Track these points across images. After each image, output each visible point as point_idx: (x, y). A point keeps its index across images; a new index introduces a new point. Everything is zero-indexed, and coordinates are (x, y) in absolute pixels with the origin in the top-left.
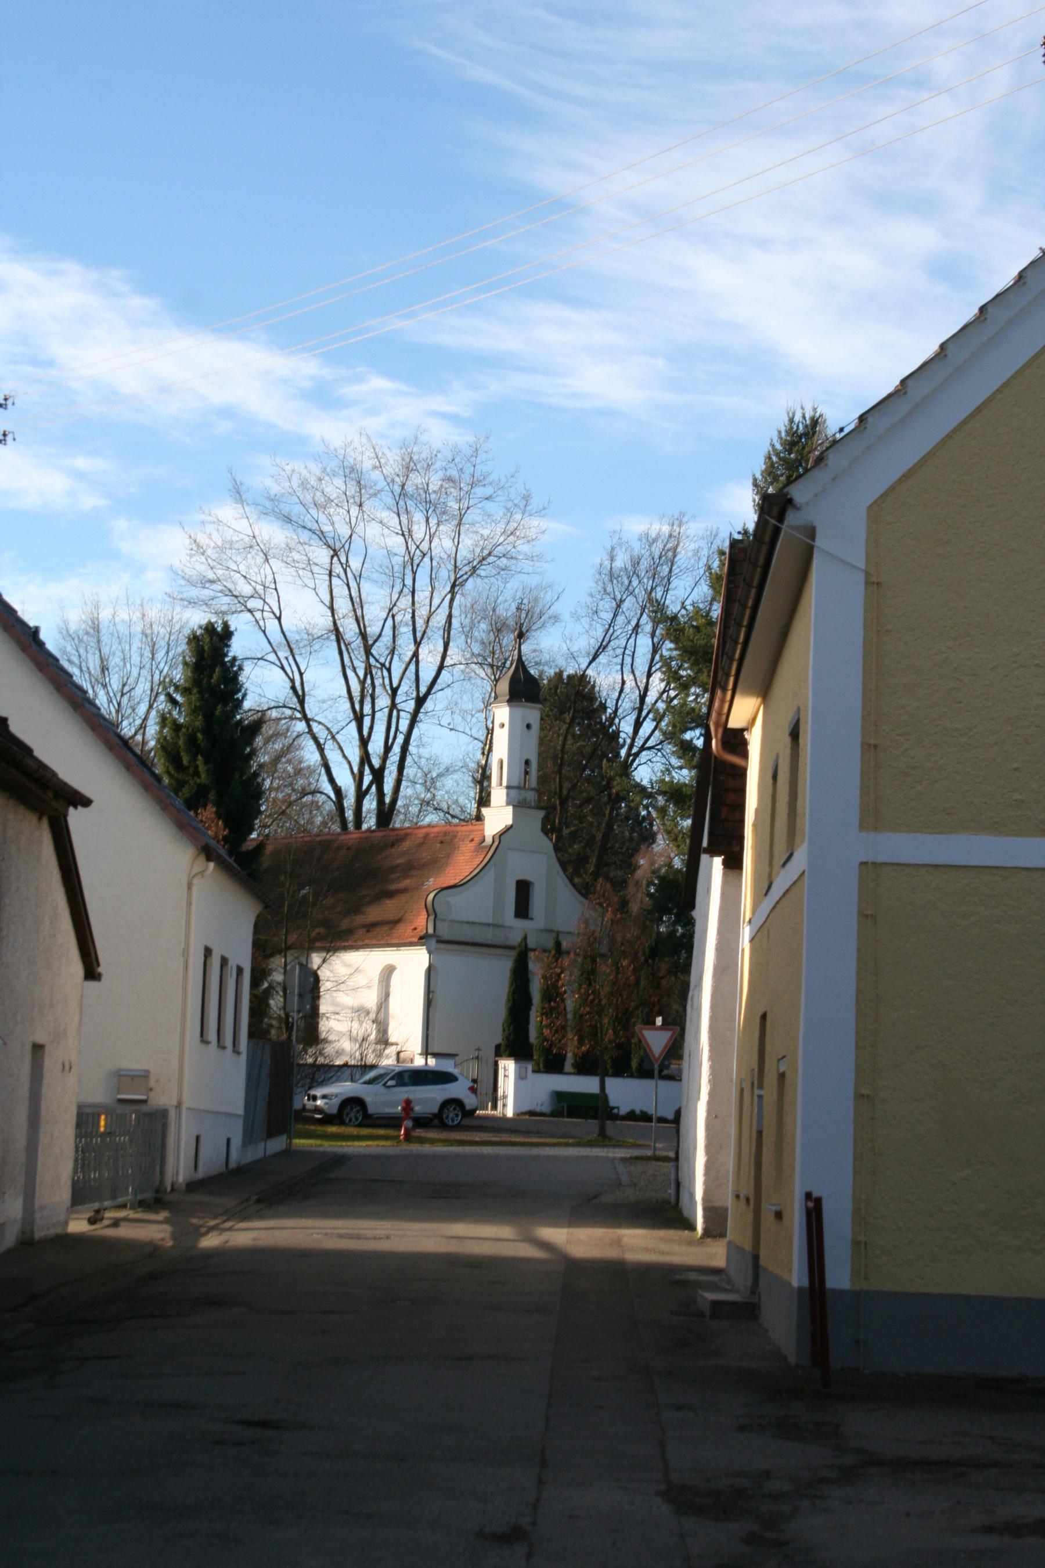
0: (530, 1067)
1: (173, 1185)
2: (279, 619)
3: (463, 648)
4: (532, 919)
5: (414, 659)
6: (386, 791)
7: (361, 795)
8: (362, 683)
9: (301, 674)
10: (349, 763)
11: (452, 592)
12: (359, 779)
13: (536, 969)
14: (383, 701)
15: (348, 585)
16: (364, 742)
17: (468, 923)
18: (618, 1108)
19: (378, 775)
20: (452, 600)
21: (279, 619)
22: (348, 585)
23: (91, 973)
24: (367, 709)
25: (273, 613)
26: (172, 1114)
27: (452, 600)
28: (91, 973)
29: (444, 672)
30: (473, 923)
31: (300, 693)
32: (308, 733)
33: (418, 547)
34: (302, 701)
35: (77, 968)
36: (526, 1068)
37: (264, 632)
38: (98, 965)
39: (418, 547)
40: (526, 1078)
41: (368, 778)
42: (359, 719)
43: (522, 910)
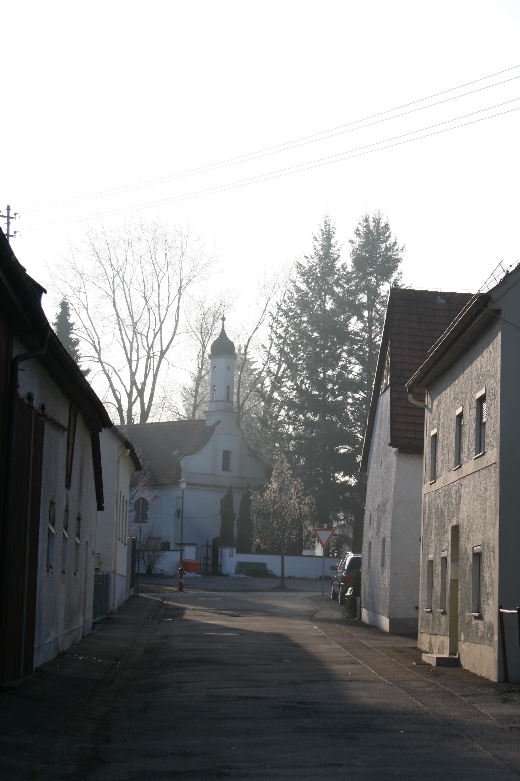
0: (235, 550)
1: (111, 611)
2: (87, 309)
3: (198, 328)
4: (232, 471)
5: (160, 331)
6: (145, 402)
7: (131, 404)
8: (131, 343)
9: (98, 339)
10: (124, 386)
11: (180, 294)
12: (130, 395)
13: (237, 499)
14: (143, 353)
15: (124, 290)
16: (133, 375)
17: (198, 473)
18: (272, 571)
19: (141, 393)
20: (179, 298)
21: (87, 309)
22: (124, 290)
23: (100, 507)
24: (134, 358)
25: (84, 305)
26: (112, 575)
27: (179, 298)
28: (100, 507)
29: (175, 337)
30: (201, 474)
31: (98, 349)
32: (103, 370)
33: (161, 270)
34: (98, 352)
35: (95, 505)
36: (233, 551)
37: (79, 315)
38: (103, 503)
39: (161, 270)
40: (232, 556)
41: (135, 394)
42: (130, 361)
43: (226, 467)
